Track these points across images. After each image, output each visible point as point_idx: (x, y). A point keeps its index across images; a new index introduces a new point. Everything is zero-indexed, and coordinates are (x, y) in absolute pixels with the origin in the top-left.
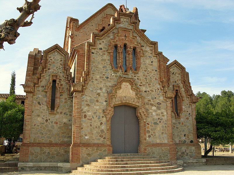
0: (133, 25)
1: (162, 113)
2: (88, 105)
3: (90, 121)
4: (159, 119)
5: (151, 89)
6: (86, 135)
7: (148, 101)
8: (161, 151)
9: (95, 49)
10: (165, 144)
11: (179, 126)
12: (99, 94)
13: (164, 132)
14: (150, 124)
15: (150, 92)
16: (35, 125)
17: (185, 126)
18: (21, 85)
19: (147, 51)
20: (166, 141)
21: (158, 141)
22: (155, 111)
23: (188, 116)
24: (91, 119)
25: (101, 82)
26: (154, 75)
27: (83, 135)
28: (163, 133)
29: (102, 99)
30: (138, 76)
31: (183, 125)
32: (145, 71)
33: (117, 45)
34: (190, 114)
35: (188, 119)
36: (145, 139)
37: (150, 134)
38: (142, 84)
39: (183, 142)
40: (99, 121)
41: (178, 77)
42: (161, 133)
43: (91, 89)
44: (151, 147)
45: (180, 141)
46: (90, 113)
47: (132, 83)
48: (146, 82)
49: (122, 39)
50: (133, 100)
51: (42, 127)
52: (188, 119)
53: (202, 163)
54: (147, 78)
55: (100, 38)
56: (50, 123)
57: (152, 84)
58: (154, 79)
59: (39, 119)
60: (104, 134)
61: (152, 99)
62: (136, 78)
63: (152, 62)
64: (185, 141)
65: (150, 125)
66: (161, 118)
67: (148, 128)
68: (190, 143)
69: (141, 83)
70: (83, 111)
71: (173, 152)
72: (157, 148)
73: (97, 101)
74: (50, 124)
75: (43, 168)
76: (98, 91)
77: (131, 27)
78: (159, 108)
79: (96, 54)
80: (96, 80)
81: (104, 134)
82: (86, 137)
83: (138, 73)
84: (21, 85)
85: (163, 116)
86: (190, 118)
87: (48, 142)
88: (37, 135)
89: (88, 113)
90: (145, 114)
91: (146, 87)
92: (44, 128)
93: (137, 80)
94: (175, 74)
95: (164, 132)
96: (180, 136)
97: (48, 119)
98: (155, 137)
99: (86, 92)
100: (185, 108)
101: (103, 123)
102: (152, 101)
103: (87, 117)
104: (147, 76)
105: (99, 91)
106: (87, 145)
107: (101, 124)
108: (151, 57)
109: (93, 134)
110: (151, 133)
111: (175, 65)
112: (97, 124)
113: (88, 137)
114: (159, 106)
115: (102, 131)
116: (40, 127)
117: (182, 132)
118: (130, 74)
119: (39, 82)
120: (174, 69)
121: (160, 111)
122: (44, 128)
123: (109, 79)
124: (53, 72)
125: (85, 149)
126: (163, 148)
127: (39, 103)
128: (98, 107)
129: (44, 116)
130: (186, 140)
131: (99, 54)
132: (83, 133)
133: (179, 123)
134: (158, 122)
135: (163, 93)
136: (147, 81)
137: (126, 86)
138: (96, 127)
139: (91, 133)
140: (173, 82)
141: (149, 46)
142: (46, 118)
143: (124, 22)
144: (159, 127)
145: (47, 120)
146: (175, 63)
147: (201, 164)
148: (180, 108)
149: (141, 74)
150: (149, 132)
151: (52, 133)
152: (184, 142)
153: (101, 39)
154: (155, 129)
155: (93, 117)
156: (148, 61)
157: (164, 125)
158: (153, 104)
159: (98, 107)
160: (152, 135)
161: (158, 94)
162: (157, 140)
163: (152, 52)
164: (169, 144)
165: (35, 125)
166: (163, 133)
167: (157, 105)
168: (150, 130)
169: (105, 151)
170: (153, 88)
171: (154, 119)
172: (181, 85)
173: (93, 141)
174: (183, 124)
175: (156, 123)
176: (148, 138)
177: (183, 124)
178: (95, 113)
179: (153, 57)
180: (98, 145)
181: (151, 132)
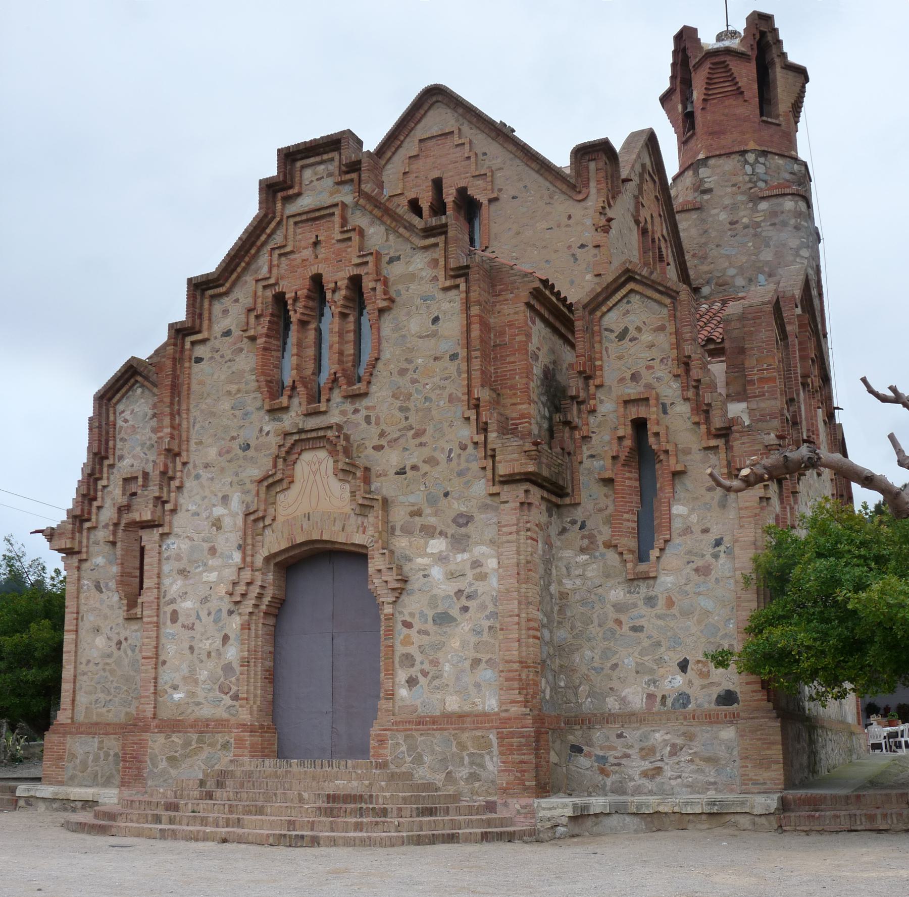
0: (352, 180)
1: (476, 564)
2: (183, 572)
3: (191, 633)
4: (459, 593)
5: (426, 452)
6: (175, 688)
7: (413, 514)
8: (454, 749)
9: (204, 341)
10: (481, 719)
11: (647, 617)
12: (217, 524)
13: (485, 657)
14: (417, 624)
15: (425, 468)
16: (89, 662)
17: (686, 614)
18: (37, 532)
19: (412, 277)
20: (491, 703)
21: (453, 704)
22: (441, 559)
23: (708, 557)
24: (194, 624)
25: (222, 470)
26: (446, 379)
27: (166, 687)
28: (476, 662)
29: (227, 540)
30: (367, 408)
31: (675, 611)
32: (402, 372)
33: (284, 293)
34: (718, 543)
35: (703, 571)
36: (391, 696)
37: (414, 671)
38: (383, 442)
39: (669, 702)
40: (219, 631)
41: (651, 346)
42: (467, 664)
43: (194, 508)
44: (406, 730)
45: (651, 697)
46: (188, 604)
47: (337, 443)
48: (404, 424)
49: (303, 260)
50: (338, 526)
51: (108, 668)
52: (703, 571)
53: (748, 817)
54: (411, 405)
55: (222, 290)
56: (129, 652)
57: (430, 430)
58: (442, 403)
59: (100, 641)
60: (233, 679)
61: (432, 501)
62: (360, 417)
63: (436, 320)
64: (683, 699)
65: (416, 627)
66: (472, 589)
67: (407, 642)
68: (713, 706)
69: (382, 434)
70: (167, 599)
71: (517, 758)
72: (437, 733)
73: (213, 551)
74: (127, 655)
75: (79, 804)
76: (214, 509)
77: (347, 196)
78: (460, 543)
79: (212, 358)
80: (207, 466)
81: (233, 679)
82: (177, 696)
83: (365, 395)
84: (37, 532)
85: (482, 577)
86: (722, 566)
87: (122, 718)
88: (94, 697)
89: (183, 605)
90: (386, 582)
91: (405, 449)
92: (112, 672)
93: (364, 425)
94: (632, 332)
95: (485, 657)
96: (652, 671)
97: (122, 639)
98: (436, 682)
99: (180, 522)
100: (692, 510)
101: (232, 636)
102: (428, 511)
103: (182, 619)
104: (409, 396)
105: (219, 511)
106: (172, 726)
107: (226, 638)
108: (433, 298)
109: (196, 682)
110: (418, 667)
111: (631, 286)
112: (210, 645)
113: (182, 695)
114: (463, 530)
115: (228, 668)
116: (100, 666)
117: (663, 649)
118: (337, 411)
119: (94, 510)
120: (628, 312)
121: (466, 556)
122: (112, 672)
123: (250, 453)
124: (132, 466)
125: (161, 739)
126: (465, 736)
127: (98, 588)
128: (213, 576)
129: (111, 628)
130: (688, 691)
131: (222, 356)
132: (167, 676)
133: (650, 601)
134: (455, 612)
135: (484, 463)
136: (407, 418)
137: (315, 466)
138: (209, 654)
139: (191, 678)
140: (622, 380)
141: (426, 248)
142: (118, 633)
143: (318, 180)
144: (460, 638)
145: (119, 643)
146: (631, 279)
147: (744, 821)
148: (505, 529)
149: (380, 393)
150: (408, 660)
151: (134, 687)
152: (676, 700)
153: (226, 294)
154: (438, 647)
155: (198, 617)
156: (416, 324)
157: (486, 624)
158: (435, 528)
159: (213, 576)
160: (425, 674)
161: (461, 474)
162: (449, 699)
163: (434, 272)
164: (503, 715)
165: (89, 662)
166: (476, 662)
167: (452, 530)
168: (413, 650)
169: (225, 746)
170: (435, 449)
171: (433, 601)
172: (670, 390)
173: (196, 709)
174: (670, 603)
175: (443, 619)
176: (403, 692)
177: (670, 603)
178: (205, 600)
179: (440, 295)
180: (205, 727)
181: (417, 663)
